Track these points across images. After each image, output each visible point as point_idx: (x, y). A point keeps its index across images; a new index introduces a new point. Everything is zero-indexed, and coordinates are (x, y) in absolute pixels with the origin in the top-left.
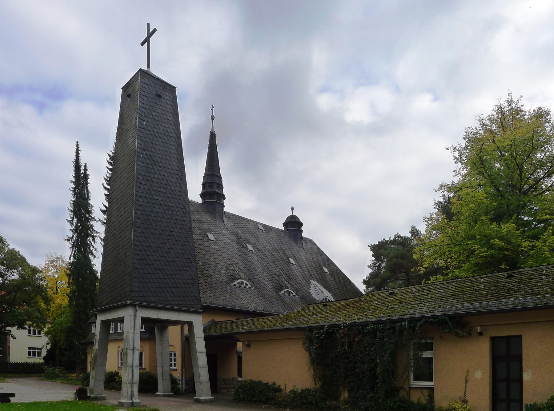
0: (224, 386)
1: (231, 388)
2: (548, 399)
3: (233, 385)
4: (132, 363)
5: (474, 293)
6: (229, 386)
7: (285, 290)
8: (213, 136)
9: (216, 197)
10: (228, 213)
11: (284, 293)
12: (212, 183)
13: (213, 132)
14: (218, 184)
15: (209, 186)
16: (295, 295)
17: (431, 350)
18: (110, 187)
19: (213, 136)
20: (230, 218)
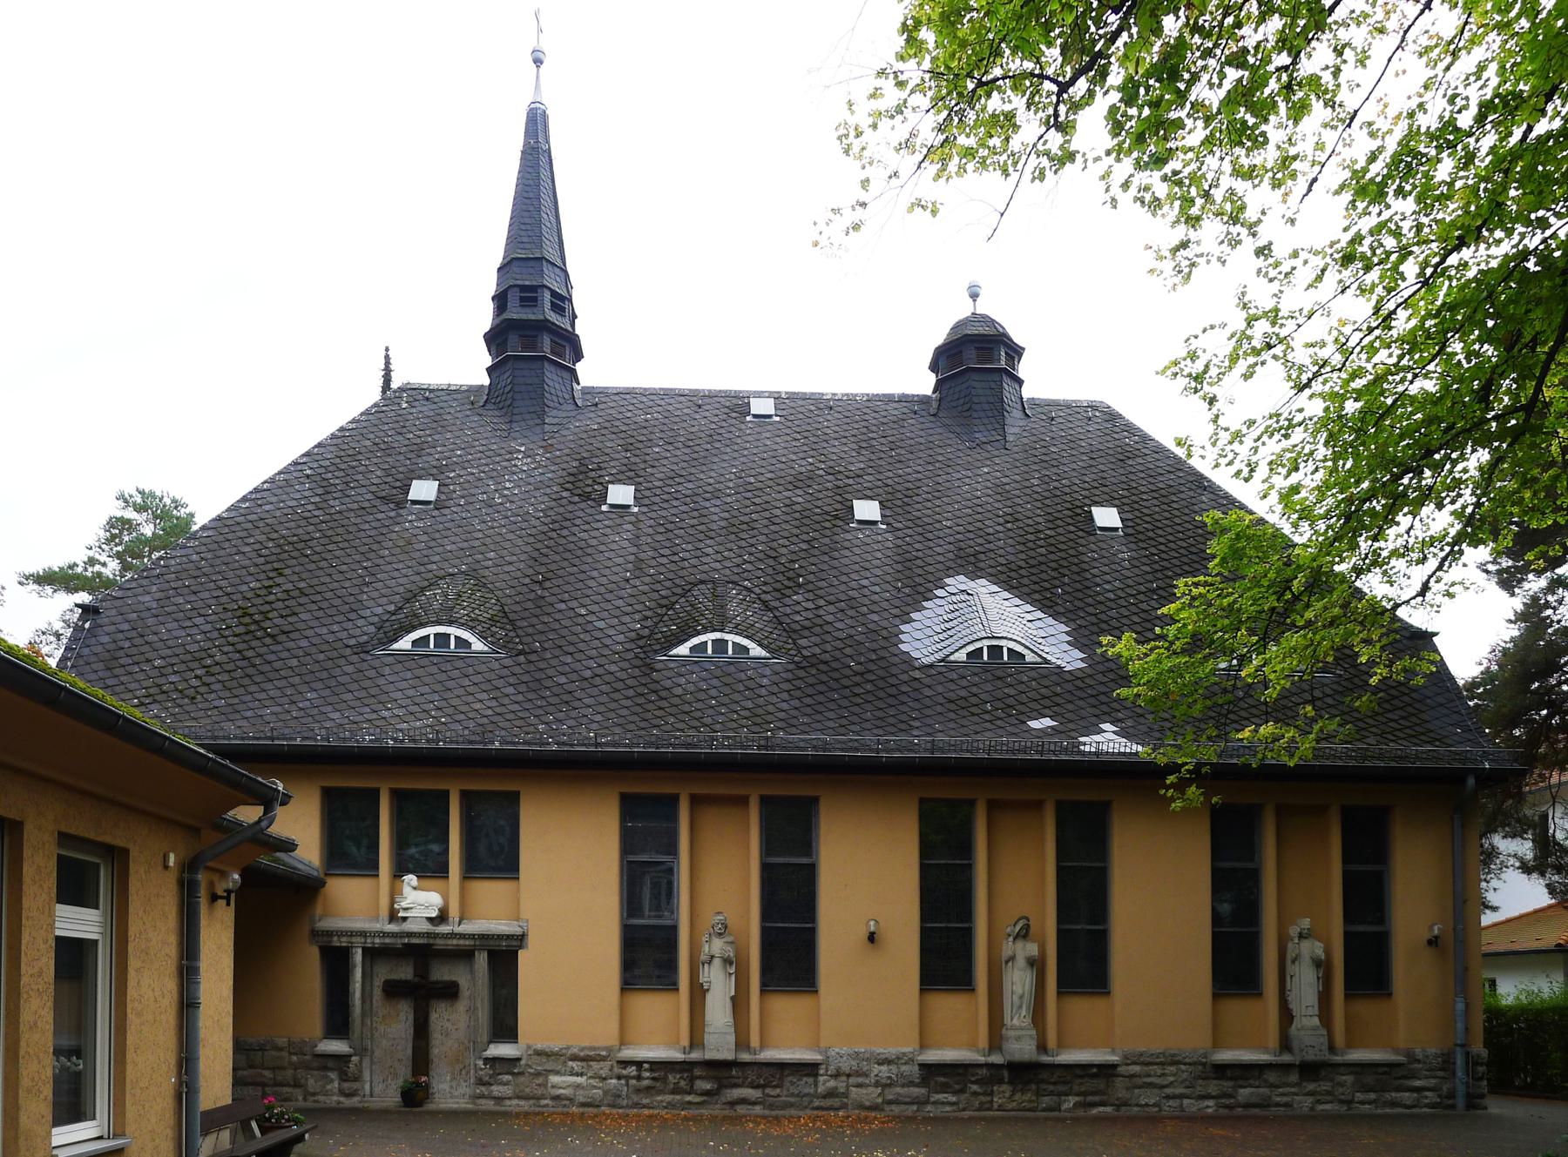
0: (245, 1073)
1: (283, 1085)
2: (1163, 372)
3: (290, 1073)
4: (133, 930)
5: (758, 1109)
6: (267, 1073)
7: (695, 641)
8: (536, 123)
9: (546, 342)
10: (603, 392)
11: (409, 646)
12: (533, 289)
13: (538, 105)
14: (554, 294)
15: (522, 299)
16: (764, 653)
17: (1500, 1022)
18: (883, 506)
19: (536, 123)
20: (596, 405)
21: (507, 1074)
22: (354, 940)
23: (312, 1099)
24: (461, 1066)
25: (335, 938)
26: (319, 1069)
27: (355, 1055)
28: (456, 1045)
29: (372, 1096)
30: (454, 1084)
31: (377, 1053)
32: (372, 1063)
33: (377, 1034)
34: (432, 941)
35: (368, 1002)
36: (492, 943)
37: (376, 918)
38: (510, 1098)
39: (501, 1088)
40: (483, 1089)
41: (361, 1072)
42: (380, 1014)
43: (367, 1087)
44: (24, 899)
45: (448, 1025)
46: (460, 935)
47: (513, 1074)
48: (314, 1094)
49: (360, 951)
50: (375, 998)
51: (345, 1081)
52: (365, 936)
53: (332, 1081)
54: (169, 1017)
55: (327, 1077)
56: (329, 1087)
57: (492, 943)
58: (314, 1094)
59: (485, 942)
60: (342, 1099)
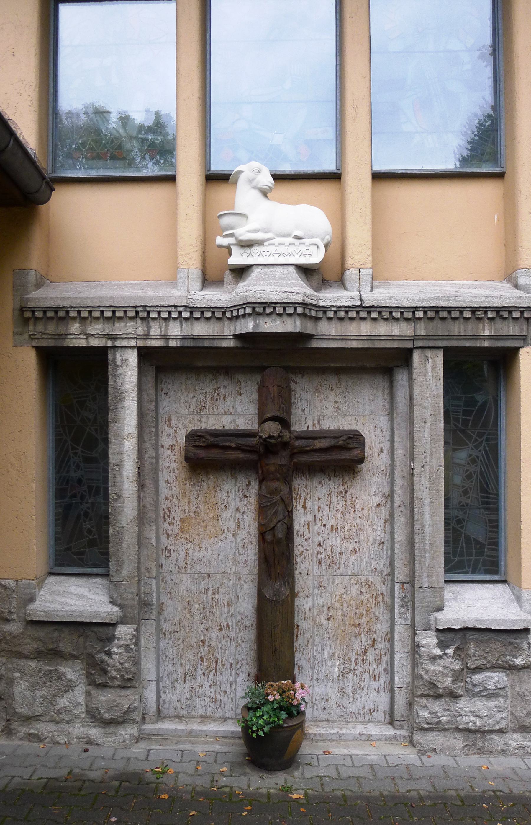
21: (495, 668)
22: (119, 328)
23: (24, 730)
24: (366, 640)
25: (75, 327)
26: (39, 655)
27: (123, 621)
28: (354, 590)
29: (160, 715)
30: (349, 683)
31: (169, 611)
32: (160, 634)
33: (169, 565)
34: (310, 328)
35: (150, 488)
36: (456, 329)
37: (173, 281)
38: (502, 731)
39: (479, 704)
40: (437, 707)
41: (137, 663)
42: (177, 514)
43: (150, 694)
44: (522, 554)
45: (334, 540)
46: (379, 309)
47: (510, 668)
48: (27, 719)
49: (132, 357)
50: (165, 476)
51: (103, 686)
52: (146, 320)
53: (70, 686)
54: (437, 346)
55: (61, 676)
56: (63, 702)
57: (456, 329)
58: (27, 719)
59: (440, 329)
60: (95, 732)
